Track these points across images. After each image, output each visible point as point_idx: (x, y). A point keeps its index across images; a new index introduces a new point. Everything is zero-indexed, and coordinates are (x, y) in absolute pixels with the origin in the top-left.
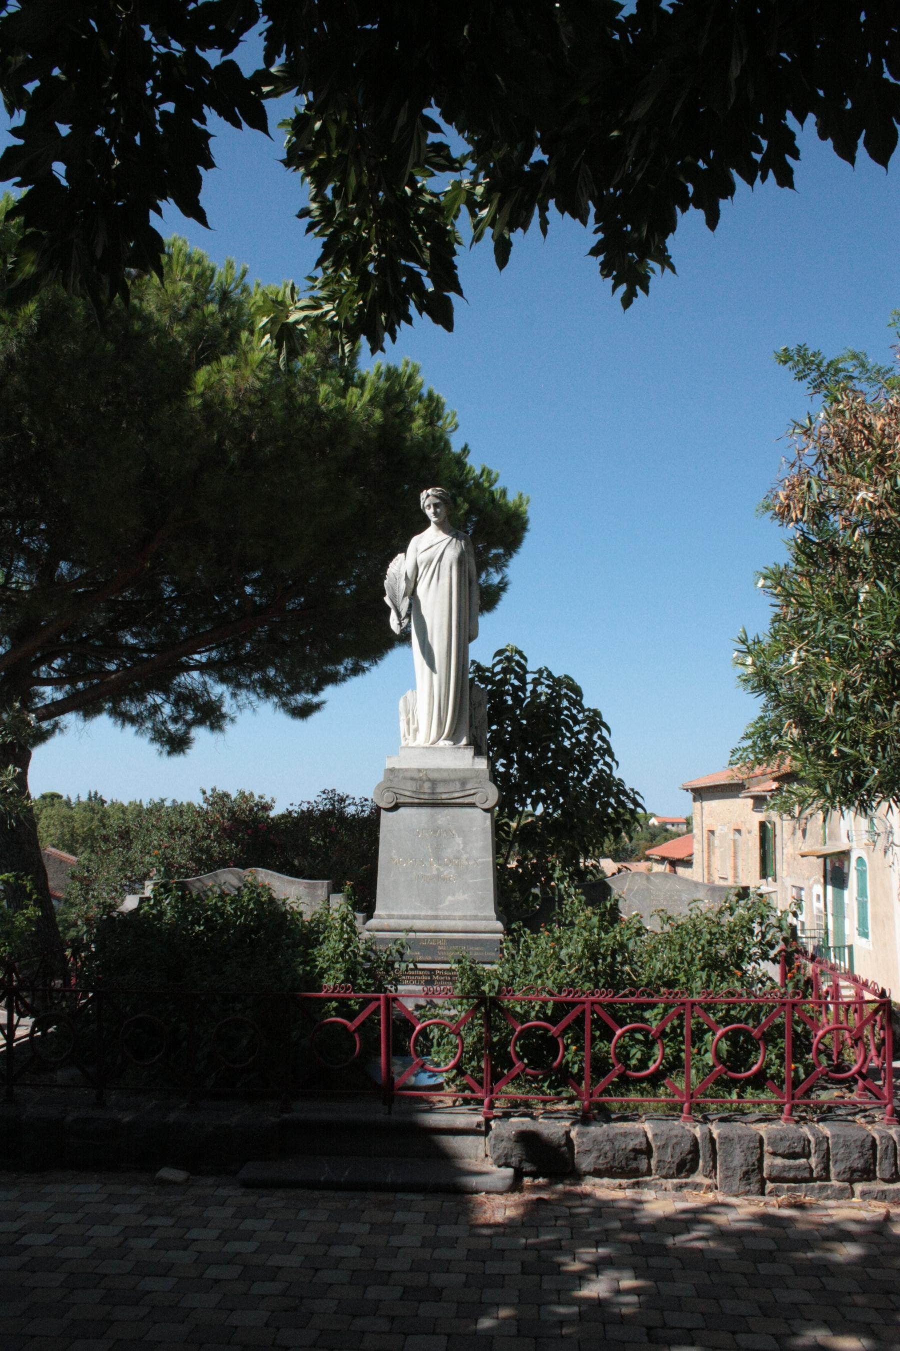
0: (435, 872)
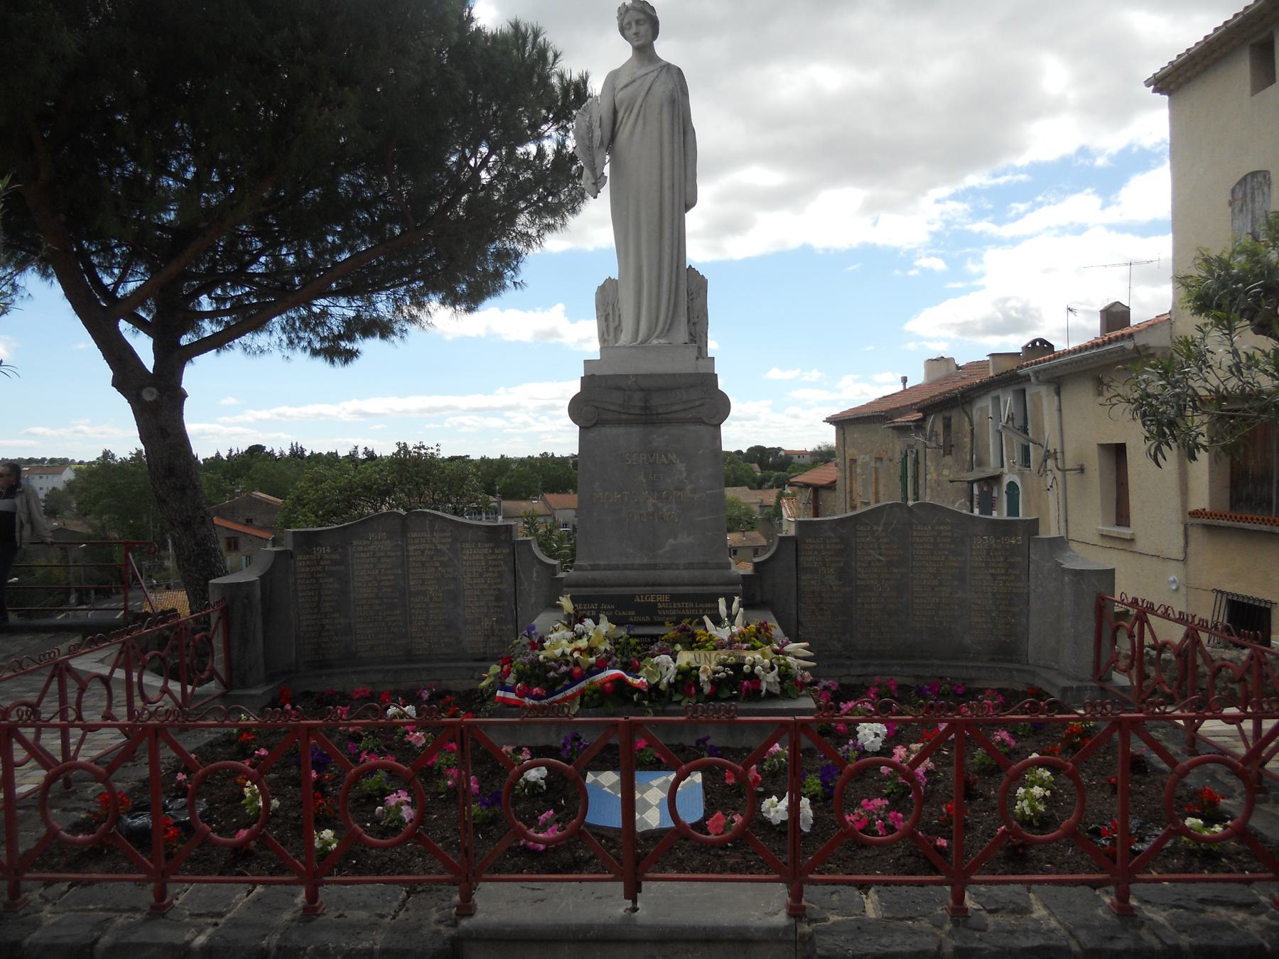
0: (651, 509)
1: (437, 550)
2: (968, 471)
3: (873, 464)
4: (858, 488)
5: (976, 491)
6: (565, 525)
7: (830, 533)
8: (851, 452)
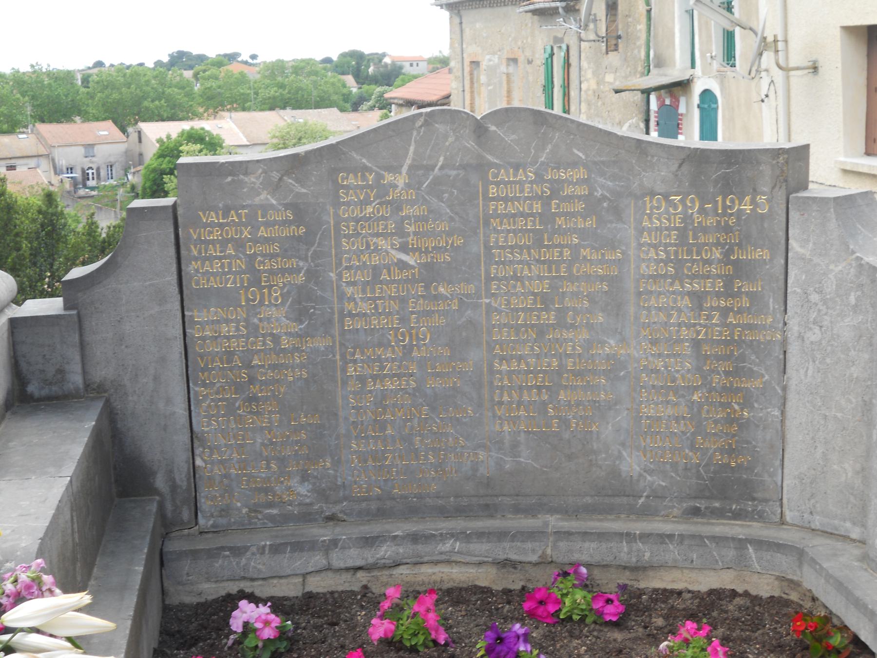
2: (643, 75)
3: (503, 68)
5: (654, 105)
6: (71, 169)
7: (264, 197)
8: (472, 51)
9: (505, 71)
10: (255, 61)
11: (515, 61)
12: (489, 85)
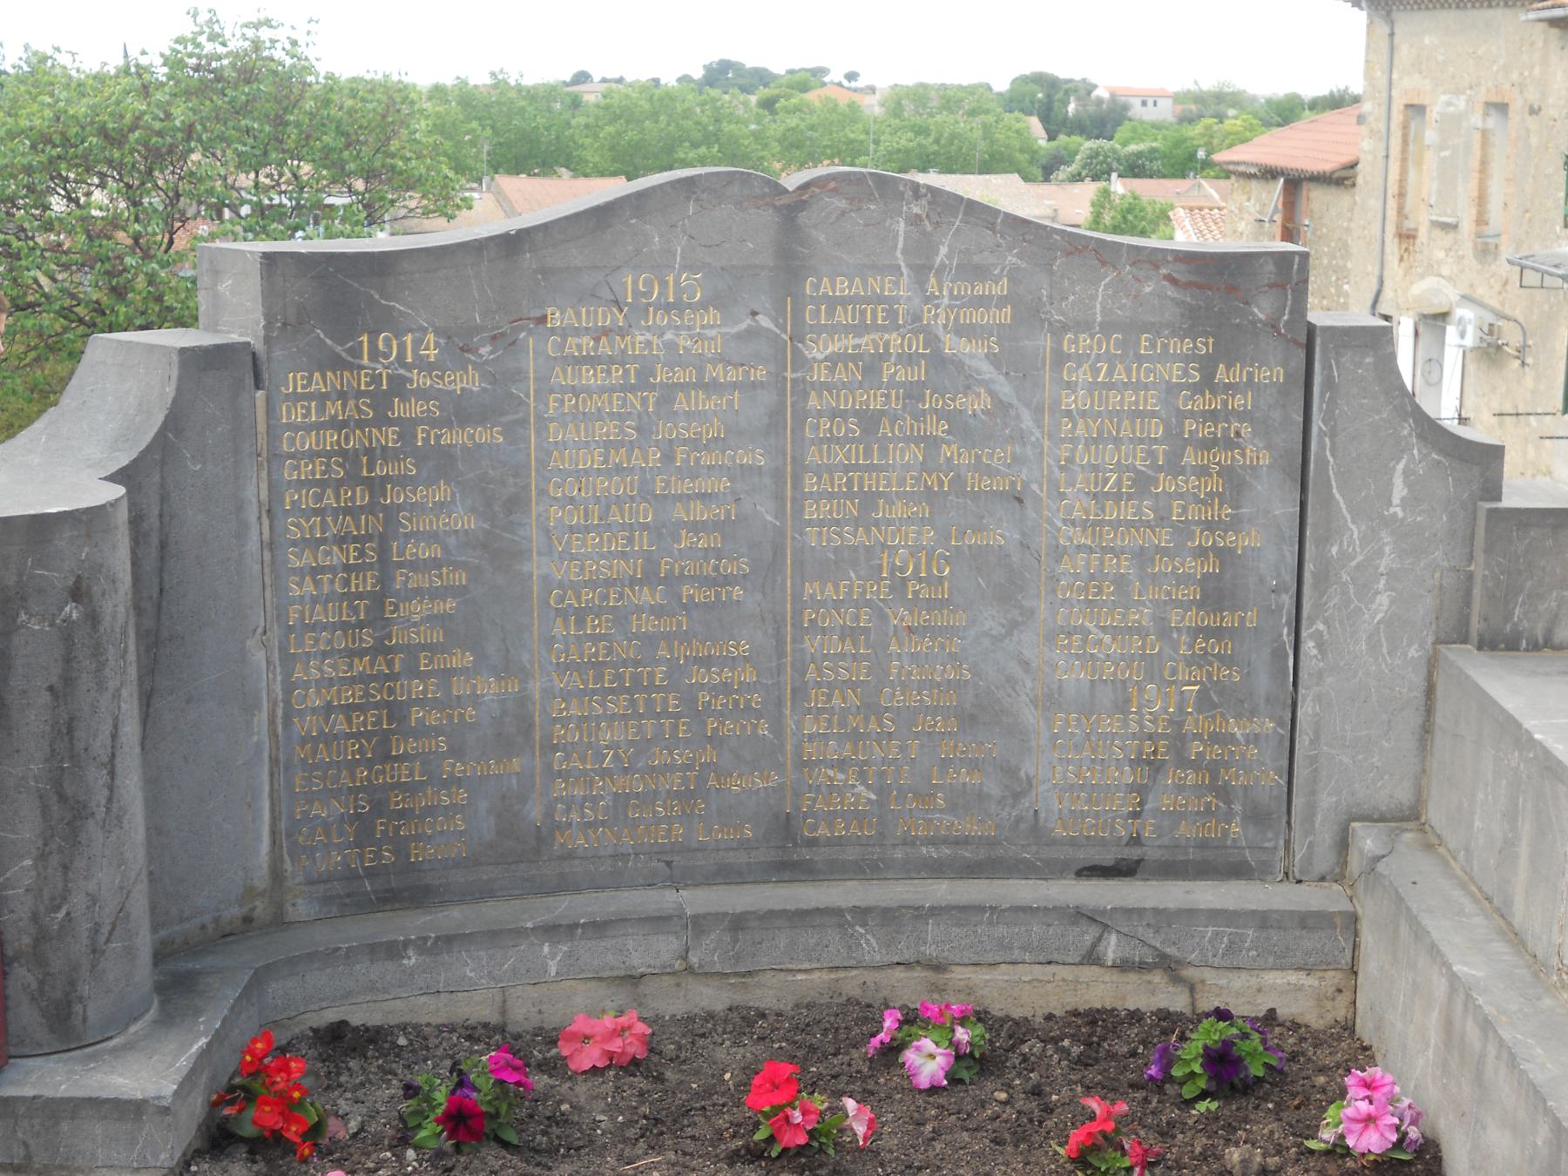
1: (938, 361)
3: (1476, 120)
4: (1425, 183)
8: (1409, 86)
9: (1480, 125)
10: (853, 84)
11: (1502, 108)
12: (1442, 148)
